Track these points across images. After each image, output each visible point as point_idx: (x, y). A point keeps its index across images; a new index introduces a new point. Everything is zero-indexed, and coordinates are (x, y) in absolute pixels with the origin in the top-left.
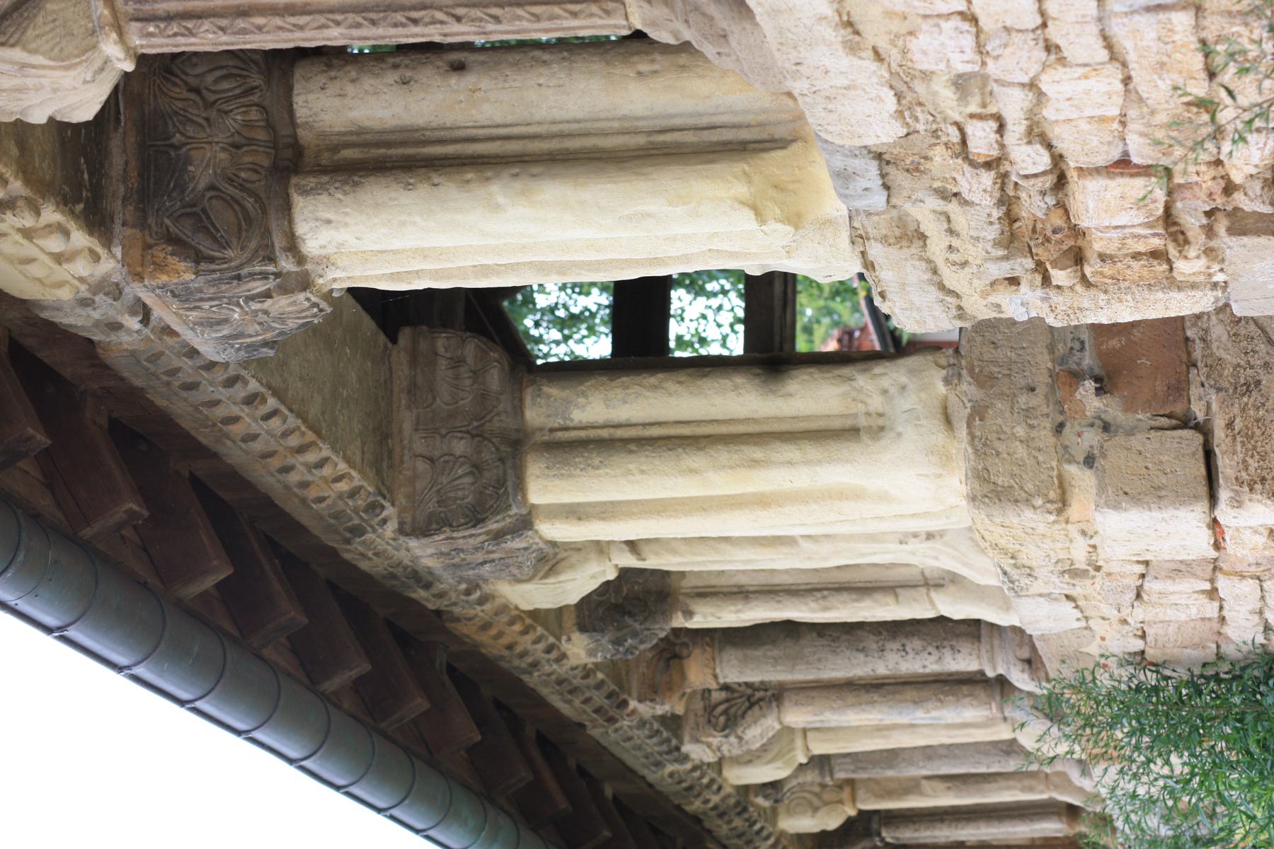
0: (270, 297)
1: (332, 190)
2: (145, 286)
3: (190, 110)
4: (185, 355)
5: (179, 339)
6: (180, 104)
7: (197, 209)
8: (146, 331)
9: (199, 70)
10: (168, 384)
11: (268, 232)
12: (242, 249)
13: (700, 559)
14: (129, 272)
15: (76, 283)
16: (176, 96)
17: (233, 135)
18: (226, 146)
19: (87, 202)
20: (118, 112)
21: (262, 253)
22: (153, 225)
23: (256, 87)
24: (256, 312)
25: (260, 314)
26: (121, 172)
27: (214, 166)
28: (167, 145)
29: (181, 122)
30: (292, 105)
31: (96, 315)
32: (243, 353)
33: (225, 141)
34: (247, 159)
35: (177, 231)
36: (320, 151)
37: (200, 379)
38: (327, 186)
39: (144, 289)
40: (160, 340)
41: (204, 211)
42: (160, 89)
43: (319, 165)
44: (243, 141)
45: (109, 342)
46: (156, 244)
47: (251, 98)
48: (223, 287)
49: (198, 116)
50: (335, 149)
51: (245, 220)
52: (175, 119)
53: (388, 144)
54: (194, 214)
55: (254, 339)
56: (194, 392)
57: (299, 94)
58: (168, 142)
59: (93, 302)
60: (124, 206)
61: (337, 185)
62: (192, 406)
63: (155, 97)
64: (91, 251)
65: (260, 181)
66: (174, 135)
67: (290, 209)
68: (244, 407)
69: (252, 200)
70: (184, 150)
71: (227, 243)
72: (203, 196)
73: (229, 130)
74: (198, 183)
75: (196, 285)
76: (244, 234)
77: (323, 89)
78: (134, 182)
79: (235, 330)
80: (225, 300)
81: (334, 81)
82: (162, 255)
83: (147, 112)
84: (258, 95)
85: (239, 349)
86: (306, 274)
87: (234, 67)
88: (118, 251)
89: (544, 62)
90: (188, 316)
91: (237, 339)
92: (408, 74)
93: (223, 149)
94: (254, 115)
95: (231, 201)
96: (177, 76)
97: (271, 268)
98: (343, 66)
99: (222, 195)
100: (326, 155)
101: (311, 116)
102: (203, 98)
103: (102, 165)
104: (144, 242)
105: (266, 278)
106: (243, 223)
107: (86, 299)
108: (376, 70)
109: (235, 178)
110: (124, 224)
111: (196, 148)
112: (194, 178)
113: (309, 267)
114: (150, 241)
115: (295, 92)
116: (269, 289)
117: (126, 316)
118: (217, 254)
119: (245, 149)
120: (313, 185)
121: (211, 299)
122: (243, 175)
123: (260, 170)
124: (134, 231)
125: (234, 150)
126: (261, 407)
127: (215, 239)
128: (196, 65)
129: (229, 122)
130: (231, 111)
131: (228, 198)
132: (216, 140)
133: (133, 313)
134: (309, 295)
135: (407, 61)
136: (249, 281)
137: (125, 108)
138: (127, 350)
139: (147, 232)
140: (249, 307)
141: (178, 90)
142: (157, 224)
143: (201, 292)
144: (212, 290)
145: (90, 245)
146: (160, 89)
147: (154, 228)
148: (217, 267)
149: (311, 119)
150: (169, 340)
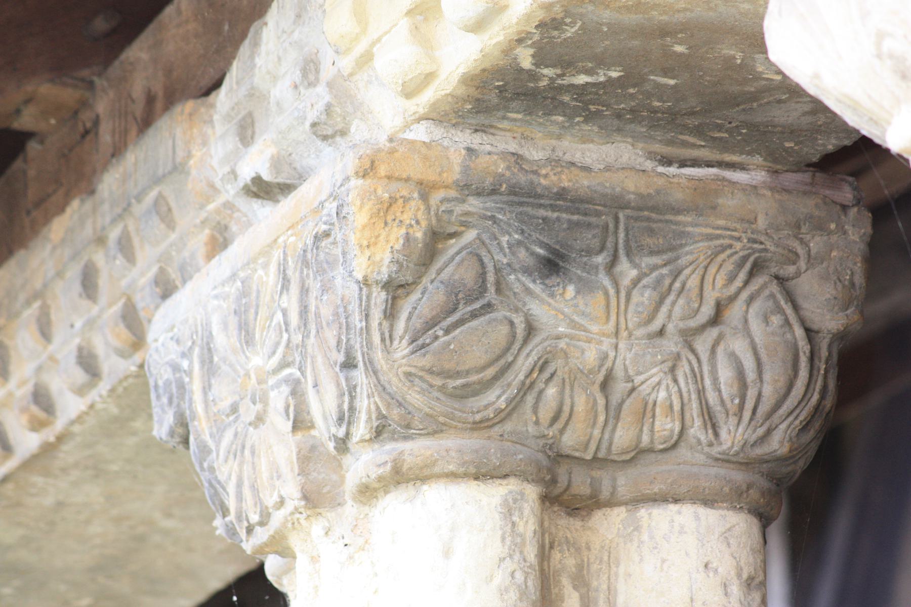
0: (296, 427)
1: (509, 566)
2: (347, 179)
3: (681, 301)
4: (162, 271)
5: (201, 260)
6: (693, 282)
7: (491, 295)
8: (230, 192)
9: (756, 326)
10: (101, 240)
11: (436, 429)
12: (408, 375)
13: (807, 409)
14: (379, 150)
15: (360, 48)
16: (709, 278)
17: (629, 379)
18: (609, 364)
19: (532, 76)
20: (683, 164)
21: (395, 413)
22: (466, 207)
23: (716, 434)
24: (264, 400)
25: (259, 406)
26: (568, 157)
27: (572, 337)
28: (616, 250)
29: (659, 281)
30: (676, 501)
31: (281, 91)
32: (167, 374)
33: (619, 362)
34: (581, 403)
35: (451, 252)
36: (578, 550)
37: (103, 299)
38: (517, 556)
39: (339, 178)
40: (203, 222)
41: (488, 307)
42: (724, 248)
43: (551, 547)
44: (615, 399)
45: (211, 122)
46: (428, 208)
47: (698, 423)
48: (330, 335)
49: (669, 317)
50: (581, 581)
51: (464, 386)
52: (665, 271)
54: (482, 289)
55: (198, 397)
56: (77, 288)
57: (697, 518)
58: (621, 252)
59: (311, 85)
60: (504, 155)
61: (519, 576)
62: (45, 286)
63: (710, 237)
64: (429, 77)
65: (537, 423)
66: (636, 266)
67: (477, 478)
68: (29, 388)
69: (502, 404)
70: (606, 282)
71: (423, 346)
72: (517, 310)
73: (639, 373)
74: (542, 301)
75: (338, 281)
76: (438, 382)
77: (706, 566)
78: (550, 180)
79: (224, 360)
80: (297, 338)
81: (720, 591)
82: (407, 218)
83: (680, 218)
84: (703, 438)
85: (176, 368)
86: (336, 503)
87: (760, 395)
88: (420, 133)
90: (266, 266)
91: (203, 363)
93: (604, 357)
94: (665, 426)
95: (502, 362)
96: (746, 283)
97: (361, 430)
99: (516, 346)
100: (571, 562)
101: (652, 538)
102: (703, 328)
103: (590, 117)
104: (434, 186)
105: (341, 419)
106: (459, 382)
107: (317, 71)
109: (546, 375)
110: (469, 150)
111: (608, 306)
112: (552, 295)
113: (350, 509)
114: (436, 197)
115: (702, 511)
116: (312, 426)
117: (271, 151)
118: (401, 325)
119: (601, 402)
120: (521, 528)
121: (304, 310)
122: (551, 391)
123: (559, 425)
124: (457, 169)
125: (600, 377)
126: (24, 419)
127: (431, 324)
128: (766, 320)
129: (656, 374)
130: (675, 381)
132: (622, 345)
133: (276, 163)
134: (290, 506)
136: (338, 384)
137: (691, 179)
138: (189, 156)
139: (453, 193)
140: (277, 385)
141: (720, 281)
142: (467, 214)
143: (325, 289)
144: (326, 312)
145: (443, 76)
146: (724, 248)
147: (459, 209)
148: (375, 324)
149: (645, 537)
150: (199, 242)
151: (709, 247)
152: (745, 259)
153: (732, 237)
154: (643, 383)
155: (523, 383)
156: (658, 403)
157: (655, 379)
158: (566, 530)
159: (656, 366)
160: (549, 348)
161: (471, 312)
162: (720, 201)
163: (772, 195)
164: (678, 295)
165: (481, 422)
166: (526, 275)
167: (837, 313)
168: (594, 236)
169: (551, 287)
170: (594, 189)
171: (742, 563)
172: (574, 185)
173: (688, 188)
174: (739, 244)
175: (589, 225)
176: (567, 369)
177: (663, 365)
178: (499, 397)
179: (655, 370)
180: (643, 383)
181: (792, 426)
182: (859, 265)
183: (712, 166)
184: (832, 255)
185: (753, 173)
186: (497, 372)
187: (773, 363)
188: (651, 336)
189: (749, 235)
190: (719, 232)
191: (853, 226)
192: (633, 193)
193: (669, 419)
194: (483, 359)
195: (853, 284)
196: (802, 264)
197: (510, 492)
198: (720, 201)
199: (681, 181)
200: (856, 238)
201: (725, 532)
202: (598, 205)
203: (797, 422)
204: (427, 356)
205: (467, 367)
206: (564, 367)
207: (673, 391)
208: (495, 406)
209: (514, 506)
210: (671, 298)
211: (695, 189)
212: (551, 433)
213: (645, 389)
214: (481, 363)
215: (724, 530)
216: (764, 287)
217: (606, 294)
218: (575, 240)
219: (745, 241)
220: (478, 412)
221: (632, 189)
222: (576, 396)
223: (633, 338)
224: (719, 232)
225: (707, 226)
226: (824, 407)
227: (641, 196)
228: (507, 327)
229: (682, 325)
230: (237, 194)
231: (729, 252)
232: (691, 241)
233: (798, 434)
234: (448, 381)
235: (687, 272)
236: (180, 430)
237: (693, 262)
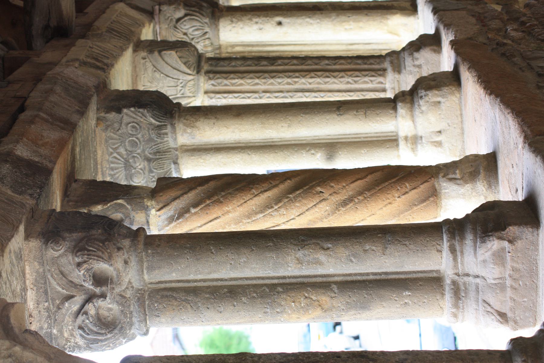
9: (187, 27)
42: (173, 34)
53: (252, 46)
87: (200, 26)
89: (311, 23)
92: (262, 26)
98: (237, 22)
102: (189, 37)
108: (250, 24)
128: (185, 25)
135: (260, 21)
141: (179, 34)
146: (173, 34)
195: (175, 8)
196: (173, 18)
204: (161, 218)
213: (202, 48)
230: (385, 86)
236: (462, 150)
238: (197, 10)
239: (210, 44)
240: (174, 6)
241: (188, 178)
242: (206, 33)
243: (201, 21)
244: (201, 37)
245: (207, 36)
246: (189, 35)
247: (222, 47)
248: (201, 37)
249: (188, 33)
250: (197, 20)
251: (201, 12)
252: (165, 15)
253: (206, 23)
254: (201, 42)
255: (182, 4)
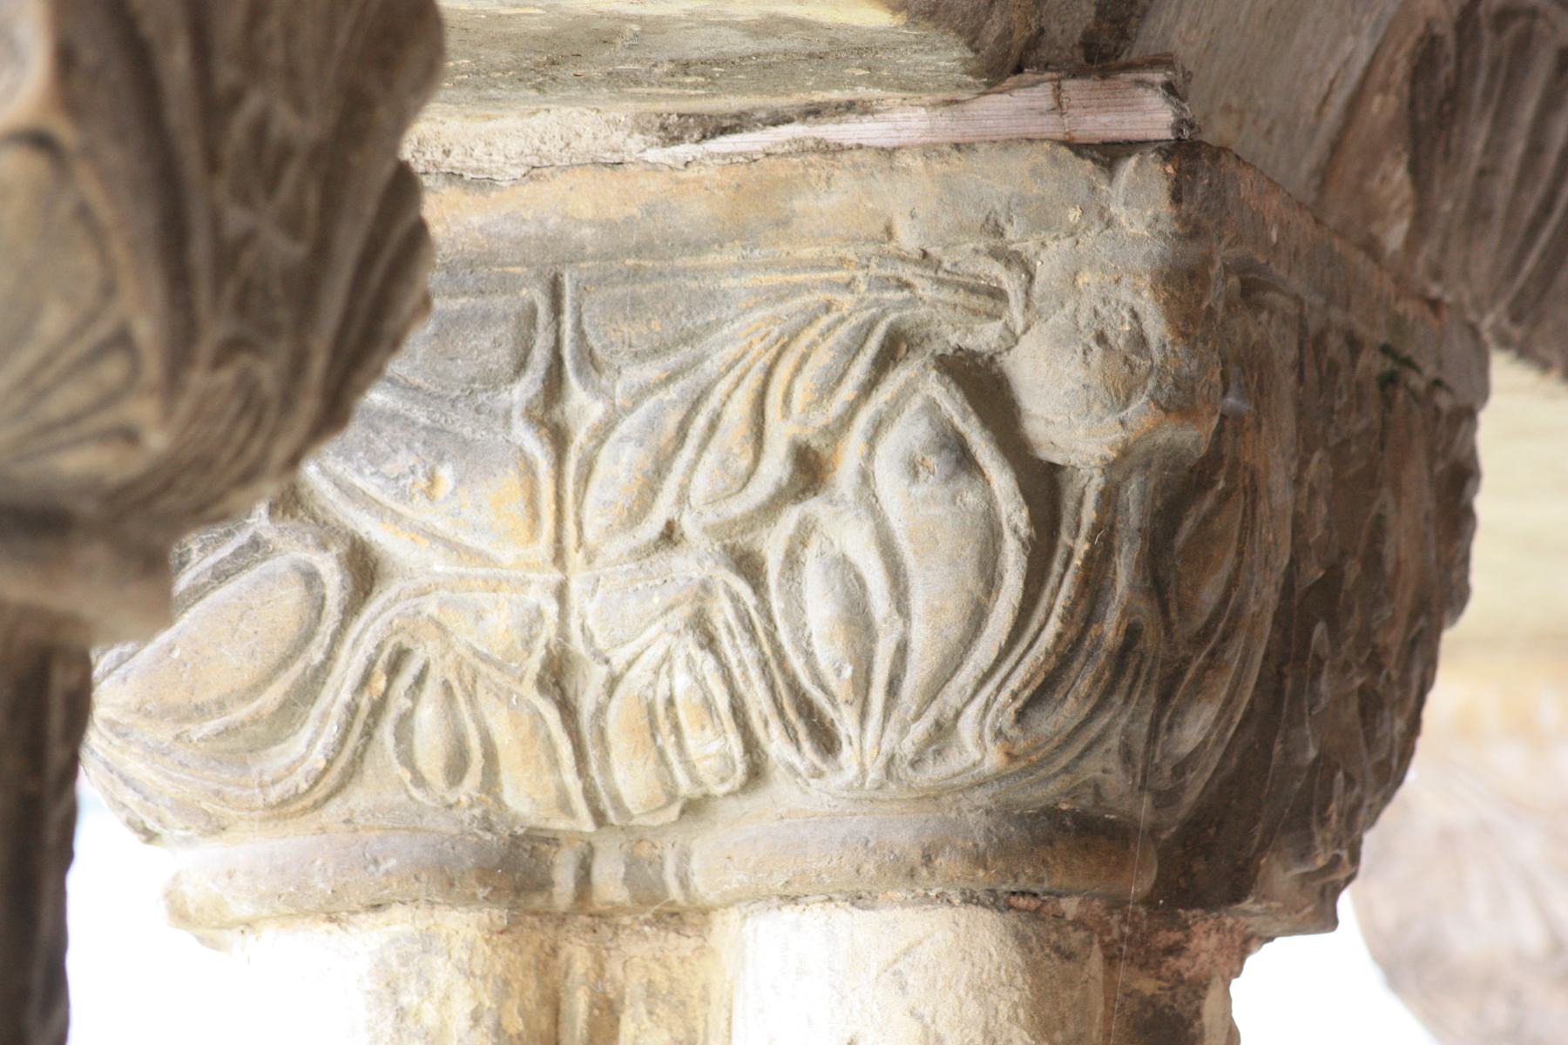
13: (1028, 660)
29: (652, 424)
32: (977, 327)
44: (586, 706)
49: (682, 498)
52: (672, 393)
58: (569, 365)
66: (599, 393)
76: (165, 733)
83: (711, 259)
87: (902, 649)
95: (297, 668)
96: (869, 387)
102: (771, 508)
109: (405, 679)
111: (532, 502)
122: (428, 714)
125: (534, 665)
131: (316, 655)
151: (775, 319)
152: (869, 328)
153: (831, 285)
154: (630, 665)
155: (352, 710)
156: (679, 700)
157: (657, 652)
158: (653, 965)
159: (653, 621)
160: (396, 622)
161: (214, 567)
162: (798, 204)
163: (926, 165)
164: (703, 446)
165: (284, 802)
166: (341, 459)
167: (1101, 419)
168: (496, 343)
169: (397, 479)
170: (494, 230)
171: (942, 1027)
172: (448, 229)
173: (719, 187)
174: (849, 297)
175: (486, 318)
176: (450, 658)
177: (670, 616)
178: (311, 744)
179: (653, 631)
180: (630, 665)
181: (996, 706)
182: (1146, 294)
183: (789, 121)
184: (1080, 281)
185: (897, 115)
186: (287, 693)
187: (928, 568)
188: (641, 554)
189: (874, 270)
190: (799, 277)
191: (1126, 204)
192: (591, 223)
193: (709, 732)
194: (248, 672)
195: (1139, 341)
196: (1015, 313)
197: (394, 941)
198: (798, 204)
199: (703, 172)
200: (1140, 229)
201: (895, 961)
202: (510, 264)
203: (1005, 695)
204: (129, 680)
205: (213, 694)
206: (443, 657)
207: (705, 668)
208: (308, 765)
209: (404, 970)
210: (687, 453)
211: (739, 186)
212: (464, 799)
214: (245, 678)
215: (891, 958)
216: (909, 389)
217: (529, 469)
218: (452, 359)
219: (863, 287)
220: (274, 783)
221: (587, 212)
222: (486, 713)
223: (598, 562)
224: (799, 277)
225: (768, 267)
226: (1100, 638)
227: (608, 226)
228: (297, 588)
229: (710, 517)
231: (825, 320)
232: (731, 313)
233: (1021, 716)
234: (187, 726)
235: (723, 386)
237: (737, 361)
238: (1110, 628)
239: (685, 787)
240: (1156, 328)
241: (65, 855)
242: (826, 740)
243: (967, 675)
244: (773, 664)
245: (776, 745)
246: (791, 517)
247: (679, 945)
248: (773, 664)
249: (814, 506)
250: (977, 618)
251: (1083, 681)
252: (1043, 222)
253: (942, 733)
254: (707, 663)
255: (1192, 437)
